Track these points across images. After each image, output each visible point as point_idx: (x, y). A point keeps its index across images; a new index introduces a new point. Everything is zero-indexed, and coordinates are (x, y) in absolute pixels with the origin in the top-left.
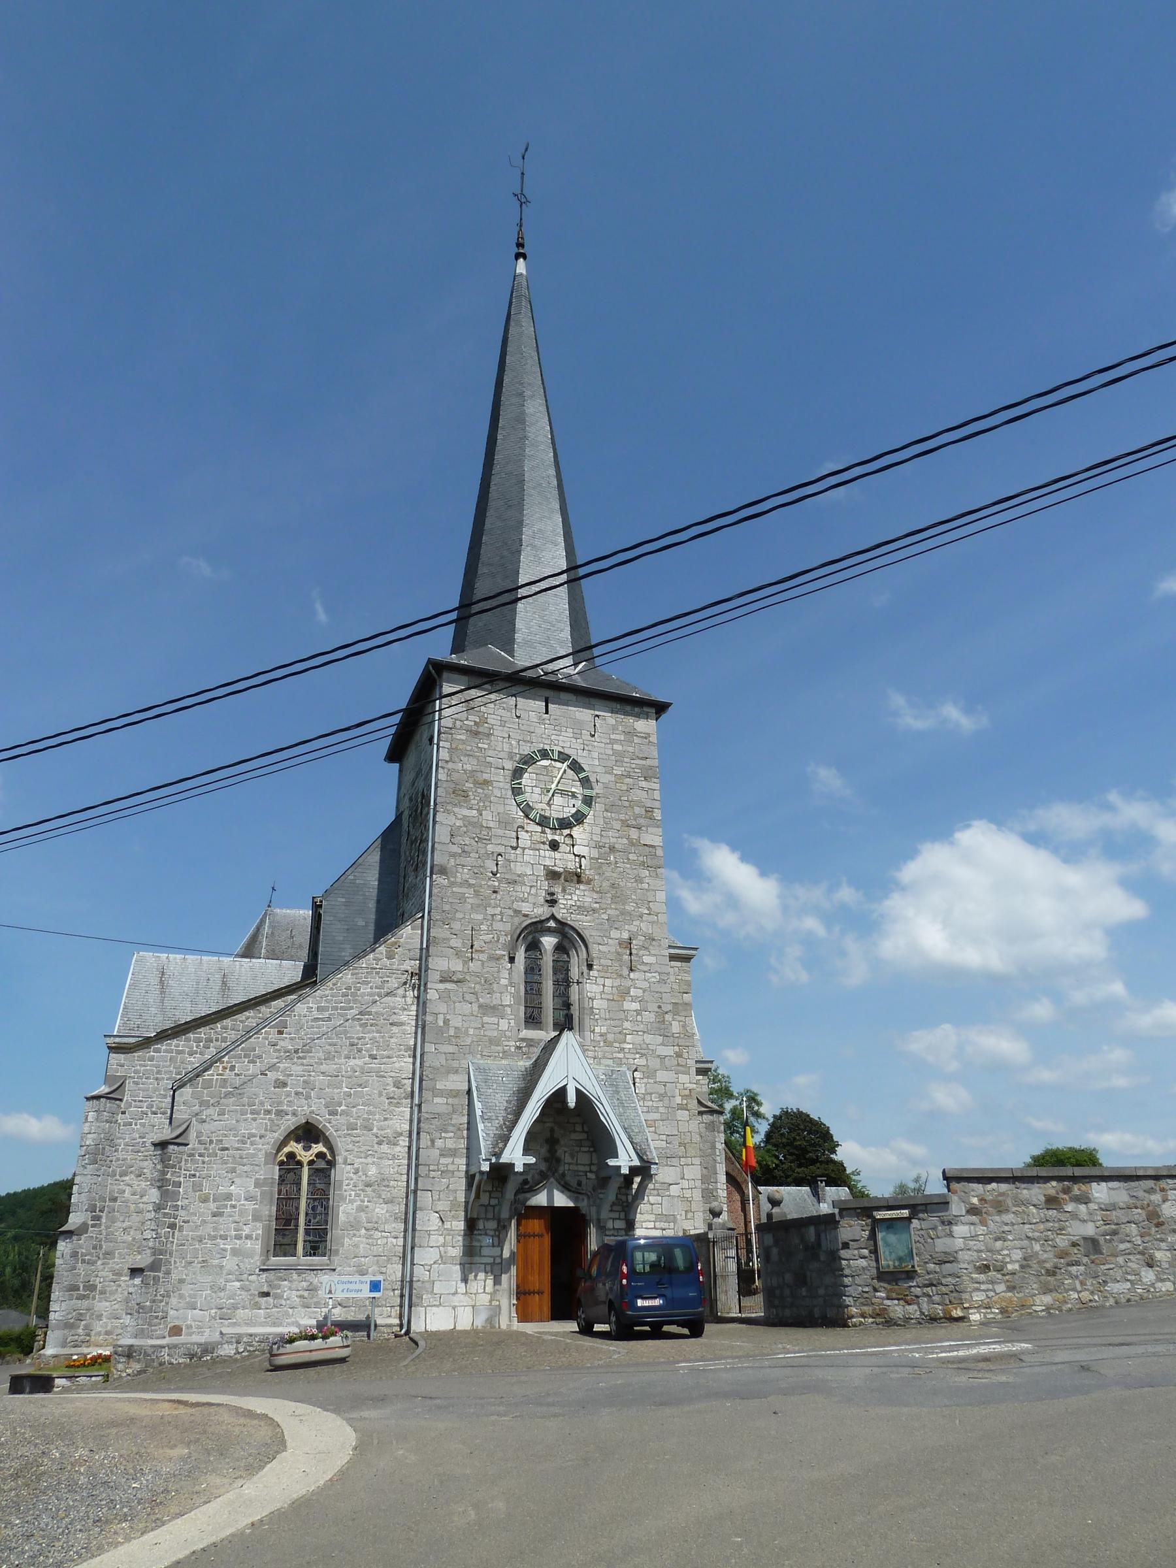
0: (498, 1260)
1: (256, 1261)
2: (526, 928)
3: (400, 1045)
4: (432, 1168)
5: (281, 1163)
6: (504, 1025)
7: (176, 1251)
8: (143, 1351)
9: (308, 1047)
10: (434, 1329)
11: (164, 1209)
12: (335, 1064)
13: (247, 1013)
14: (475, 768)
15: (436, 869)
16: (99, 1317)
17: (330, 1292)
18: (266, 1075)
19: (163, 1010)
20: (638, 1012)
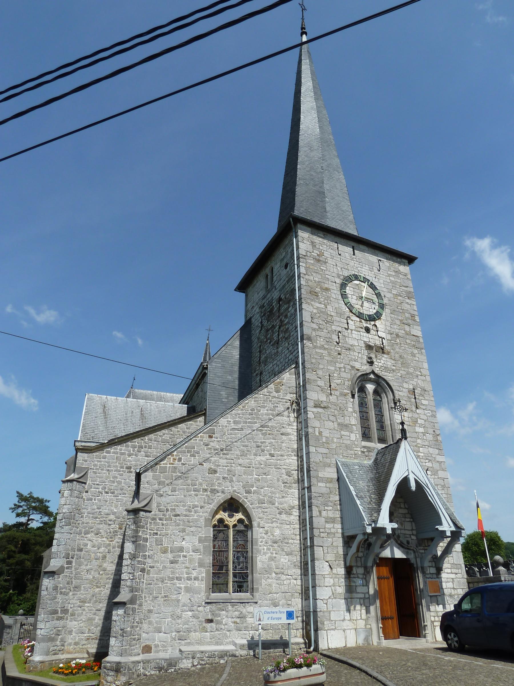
0: (367, 596)
1: (202, 596)
2: (359, 377)
3: (289, 448)
4: (321, 530)
5: (214, 526)
6: (353, 437)
7: (146, 589)
8: (127, 667)
9: (229, 447)
10: (333, 647)
11: (138, 558)
12: (248, 459)
13: (163, 431)
14: (320, 280)
15: (305, 337)
16: (70, 632)
17: (260, 620)
18: (203, 465)
19: (107, 428)
20: (424, 434)
